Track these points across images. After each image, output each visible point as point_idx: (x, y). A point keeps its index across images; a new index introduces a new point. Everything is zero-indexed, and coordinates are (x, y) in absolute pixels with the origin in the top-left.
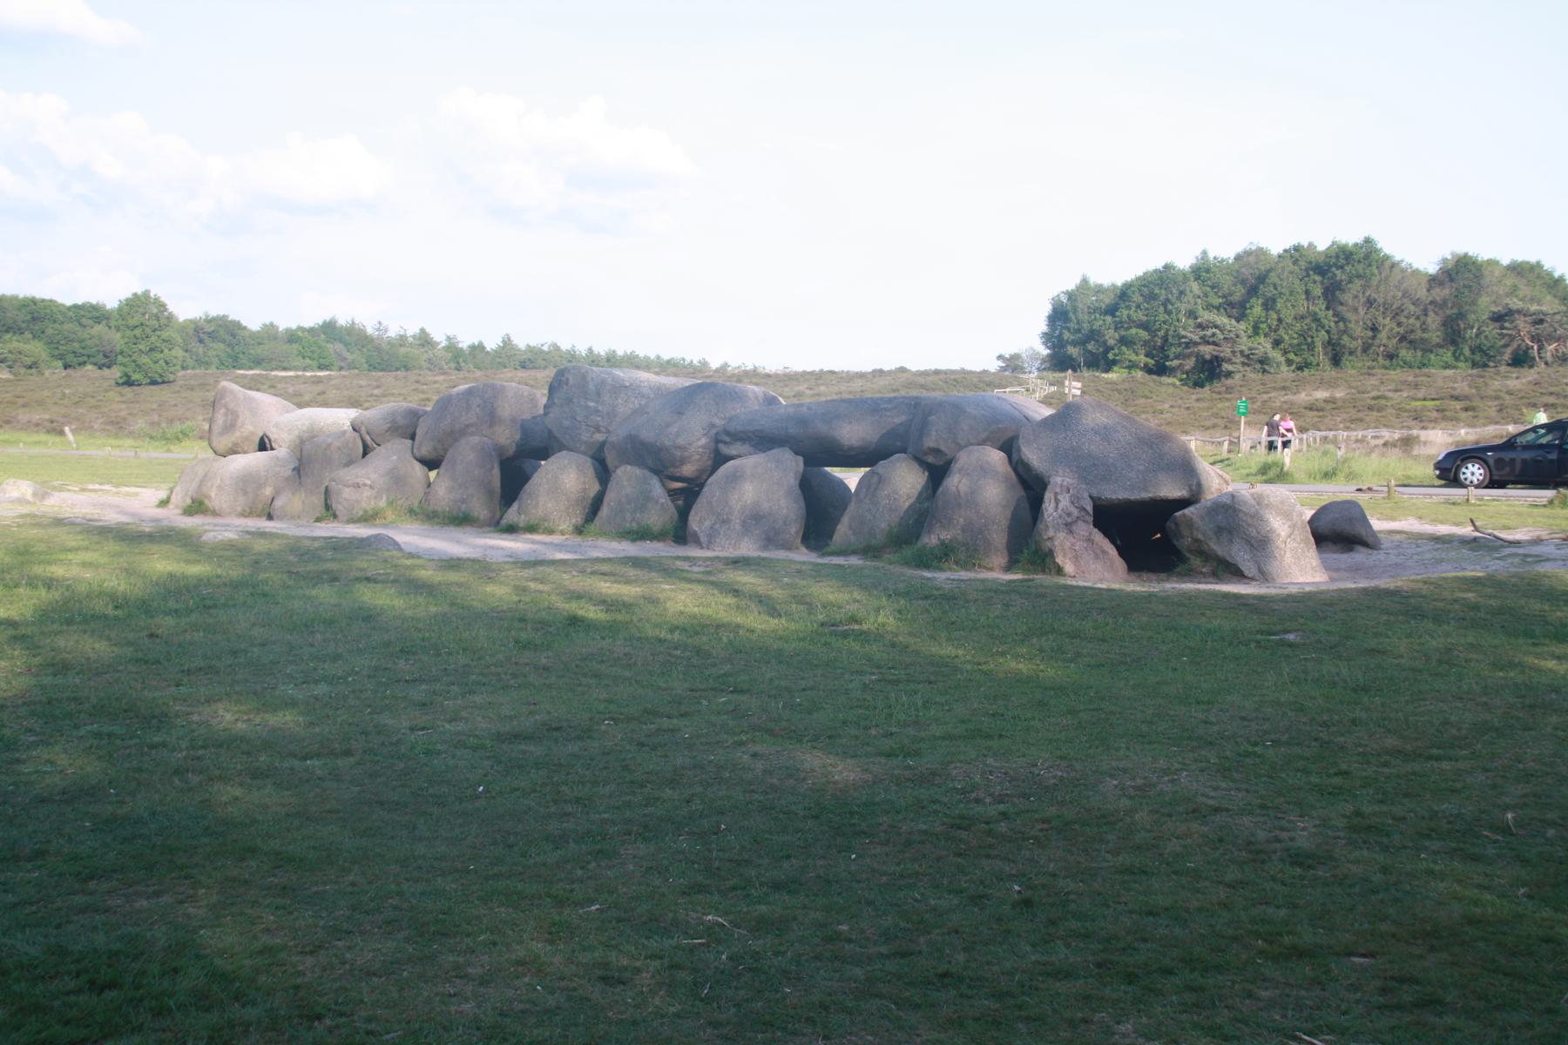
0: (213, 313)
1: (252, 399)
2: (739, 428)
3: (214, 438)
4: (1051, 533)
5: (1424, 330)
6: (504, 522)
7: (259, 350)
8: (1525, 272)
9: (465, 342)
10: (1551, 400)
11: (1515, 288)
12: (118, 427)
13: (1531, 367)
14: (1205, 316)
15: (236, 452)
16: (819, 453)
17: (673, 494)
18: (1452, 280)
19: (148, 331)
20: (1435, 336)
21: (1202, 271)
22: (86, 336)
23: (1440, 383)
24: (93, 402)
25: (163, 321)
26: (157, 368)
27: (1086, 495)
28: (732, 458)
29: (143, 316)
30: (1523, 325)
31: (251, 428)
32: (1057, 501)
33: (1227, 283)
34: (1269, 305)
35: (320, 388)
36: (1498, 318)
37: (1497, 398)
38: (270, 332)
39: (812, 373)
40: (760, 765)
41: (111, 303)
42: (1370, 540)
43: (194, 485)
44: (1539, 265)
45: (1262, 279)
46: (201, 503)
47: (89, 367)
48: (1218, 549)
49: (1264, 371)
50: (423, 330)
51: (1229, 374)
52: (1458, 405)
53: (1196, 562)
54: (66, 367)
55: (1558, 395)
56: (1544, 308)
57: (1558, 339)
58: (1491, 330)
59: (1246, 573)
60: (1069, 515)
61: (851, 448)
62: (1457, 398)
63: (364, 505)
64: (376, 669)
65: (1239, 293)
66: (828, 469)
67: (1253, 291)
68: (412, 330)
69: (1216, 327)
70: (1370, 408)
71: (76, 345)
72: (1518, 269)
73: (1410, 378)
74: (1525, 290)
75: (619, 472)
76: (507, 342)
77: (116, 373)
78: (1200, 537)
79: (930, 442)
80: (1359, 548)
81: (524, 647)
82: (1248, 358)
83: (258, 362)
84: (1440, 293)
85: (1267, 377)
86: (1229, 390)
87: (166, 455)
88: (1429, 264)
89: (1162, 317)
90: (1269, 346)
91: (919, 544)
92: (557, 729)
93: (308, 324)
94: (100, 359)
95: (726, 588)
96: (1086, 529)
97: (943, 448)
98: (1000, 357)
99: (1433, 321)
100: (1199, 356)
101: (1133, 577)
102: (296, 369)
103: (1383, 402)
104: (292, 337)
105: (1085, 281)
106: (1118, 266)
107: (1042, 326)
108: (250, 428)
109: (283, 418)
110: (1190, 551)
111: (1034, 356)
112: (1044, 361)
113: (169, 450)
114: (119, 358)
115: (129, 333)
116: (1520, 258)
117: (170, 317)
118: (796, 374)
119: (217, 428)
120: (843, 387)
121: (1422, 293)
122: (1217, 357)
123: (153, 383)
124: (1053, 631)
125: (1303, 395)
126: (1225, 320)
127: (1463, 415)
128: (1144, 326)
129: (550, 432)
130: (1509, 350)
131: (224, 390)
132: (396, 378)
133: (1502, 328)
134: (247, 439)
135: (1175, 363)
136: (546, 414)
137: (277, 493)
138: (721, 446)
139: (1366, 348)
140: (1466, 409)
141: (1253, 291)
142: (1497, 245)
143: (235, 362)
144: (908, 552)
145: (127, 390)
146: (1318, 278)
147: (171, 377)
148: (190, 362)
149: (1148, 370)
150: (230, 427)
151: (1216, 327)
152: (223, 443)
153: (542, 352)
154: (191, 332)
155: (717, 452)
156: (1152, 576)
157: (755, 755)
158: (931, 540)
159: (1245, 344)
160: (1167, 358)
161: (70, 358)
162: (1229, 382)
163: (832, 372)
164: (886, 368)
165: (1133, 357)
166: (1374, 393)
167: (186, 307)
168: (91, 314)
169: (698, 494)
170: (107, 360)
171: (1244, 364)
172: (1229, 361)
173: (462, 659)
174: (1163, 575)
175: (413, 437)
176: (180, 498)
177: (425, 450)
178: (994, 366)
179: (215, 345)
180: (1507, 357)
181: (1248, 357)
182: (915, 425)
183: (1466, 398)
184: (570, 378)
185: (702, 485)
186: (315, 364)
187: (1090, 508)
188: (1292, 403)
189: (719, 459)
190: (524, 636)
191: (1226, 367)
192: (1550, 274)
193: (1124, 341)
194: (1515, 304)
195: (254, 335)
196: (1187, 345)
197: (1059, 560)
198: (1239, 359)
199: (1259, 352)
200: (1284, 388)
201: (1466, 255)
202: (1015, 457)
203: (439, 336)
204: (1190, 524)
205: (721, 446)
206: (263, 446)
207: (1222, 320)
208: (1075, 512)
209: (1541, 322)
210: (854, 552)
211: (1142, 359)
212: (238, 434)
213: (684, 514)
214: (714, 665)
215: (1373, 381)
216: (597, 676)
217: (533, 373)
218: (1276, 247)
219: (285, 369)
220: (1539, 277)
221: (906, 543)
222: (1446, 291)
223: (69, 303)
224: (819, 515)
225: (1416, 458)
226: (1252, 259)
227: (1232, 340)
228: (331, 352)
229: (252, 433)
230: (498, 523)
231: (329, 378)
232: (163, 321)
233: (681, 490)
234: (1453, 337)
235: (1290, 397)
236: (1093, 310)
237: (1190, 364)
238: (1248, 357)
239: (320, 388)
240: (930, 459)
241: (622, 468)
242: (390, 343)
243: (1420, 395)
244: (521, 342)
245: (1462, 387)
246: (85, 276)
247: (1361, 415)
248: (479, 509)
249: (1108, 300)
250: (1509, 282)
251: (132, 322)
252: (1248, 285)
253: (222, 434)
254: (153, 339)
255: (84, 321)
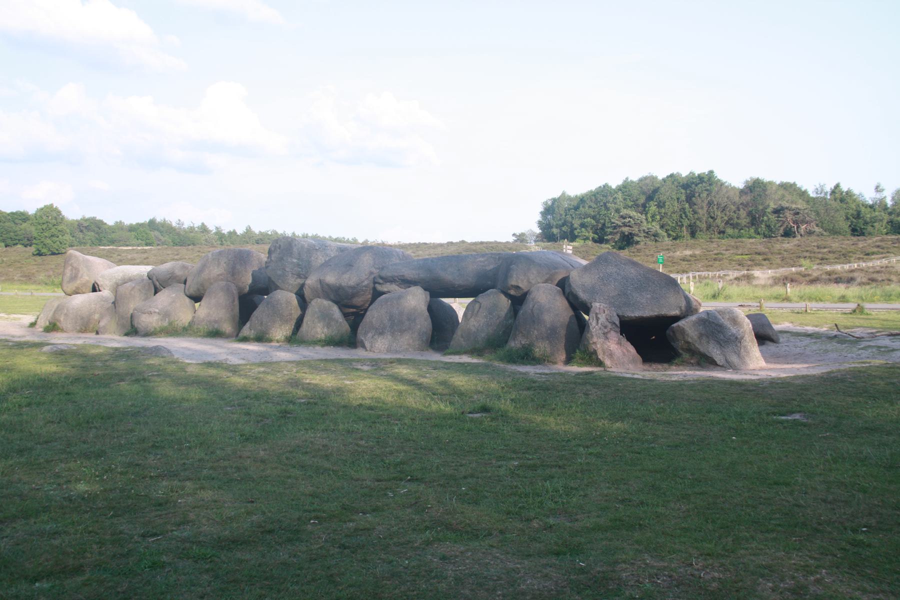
0: (87, 216)
1: (88, 261)
2: (389, 274)
3: (64, 284)
4: (595, 340)
5: (738, 218)
6: (241, 335)
7: (113, 236)
8: (788, 188)
9: (225, 231)
10: (807, 254)
11: (783, 196)
12: (28, 278)
13: (794, 237)
14: (624, 212)
15: (77, 293)
16: (438, 290)
17: (346, 315)
18: (751, 192)
19: (50, 226)
20: (744, 220)
21: (626, 187)
22: (18, 229)
23: (749, 246)
24: (19, 265)
25: (59, 220)
26: (55, 246)
27: (615, 314)
28: (384, 293)
29: (49, 217)
30: (789, 216)
31: (87, 278)
32: (598, 319)
33: (635, 193)
34: (661, 205)
35: (145, 255)
36: (777, 212)
37: (780, 254)
38: (119, 226)
39: (414, 244)
40: (450, 571)
41: (31, 210)
42: (774, 338)
43: (52, 313)
44: (794, 184)
45: (656, 191)
46: (55, 325)
47: (19, 246)
48: (702, 349)
49: (656, 241)
50: (203, 224)
51: (637, 243)
52: (760, 258)
53: (686, 356)
54: (6, 246)
55: (811, 252)
56: (799, 206)
57: (807, 223)
58: (773, 217)
59: (718, 363)
60: (606, 327)
61: (460, 286)
62: (759, 254)
63: (154, 325)
64: (130, 465)
65: (642, 200)
66: (446, 300)
67: (650, 198)
68: (197, 224)
69: (630, 217)
70: (715, 260)
71: (12, 234)
72: (785, 187)
73: (733, 244)
74: (788, 197)
75: (313, 303)
76: (249, 230)
77: (33, 249)
78: (689, 340)
79: (513, 282)
80: (768, 342)
81: (247, 439)
82: (647, 233)
83: (112, 242)
84: (747, 198)
85: (658, 244)
86: (639, 251)
87: (52, 294)
88: (740, 185)
89: (603, 212)
90: (658, 227)
91: (507, 347)
92: (270, 532)
93: (141, 221)
94: (25, 241)
95: (383, 377)
96: (614, 336)
97: (520, 285)
98: (514, 235)
99: (743, 213)
100: (623, 233)
101: (646, 367)
102: (133, 245)
103: (721, 256)
104: (132, 229)
105: (563, 194)
106: (579, 184)
107: (538, 217)
108: (86, 278)
109: (106, 271)
110: (683, 349)
111: (533, 234)
112: (537, 237)
113: (54, 291)
114: (28, 241)
115: (40, 227)
116: (785, 181)
117: (63, 218)
118: (406, 245)
119: (67, 278)
120: (432, 251)
121: (737, 199)
122: (631, 234)
123: (53, 254)
124: (628, 415)
125: (678, 253)
126: (635, 214)
127: (764, 263)
128: (594, 217)
129: (269, 278)
130: (782, 228)
131: (71, 255)
132: (188, 250)
133: (779, 217)
134: (84, 285)
135: (610, 237)
136: (267, 267)
137: (102, 317)
138: (377, 285)
139: (709, 227)
140: (765, 260)
141: (650, 198)
142: (774, 173)
143: (100, 242)
144: (501, 352)
145: (38, 258)
146: (683, 191)
147: (63, 251)
148: (76, 243)
149: (595, 241)
150: (74, 278)
151: (630, 217)
152: (70, 287)
153: (267, 235)
154: (76, 226)
155: (374, 289)
156: (659, 366)
157: (444, 558)
158: (515, 344)
159: (645, 226)
160: (605, 234)
161: (9, 242)
162: (638, 246)
163: (425, 244)
164: (454, 241)
165: (587, 234)
166: (715, 252)
167: (73, 213)
168: (22, 217)
169: (363, 316)
170: (28, 242)
171: (645, 237)
172: (637, 235)
173: (199, 453)
174: (666, 365)
175: (185, 283)
176: (43, 323)
177: (192, 291)
178: (511, 239)
179: (89, 233)
180: (781, 231)
181: (647, 233)
182: (491, 274)
183: (764, 254)
184: (283, 247)
185: (366, 310)
186: (144, 242)
187: (618, 323)
188: (673, 257)
189: (377, 294)
190: (247, 429)
191: (636, 238)
192: (799, 189)
193: (583, 225)
194: (785, 204)
195: (110, 227)
196: (615, 228)
197: (600, 357)
198: (642, 234)
199: (653, 230)
200: (668, 249)
201: (758, 179)
202: (567, 290)
203: (212, 227)
204: (682, 331)
205: (377, 285)
206: (94, 289)
207: (633, 213)
208: (610, 326)
209: (798, 213)
210: (465, 353)
211: (591, 235)
212: (78, 282)
213: (354, 327)
214: (392, 453)
215: (714, 245)
216: (303, 467)
217: (263, 246)
218: (661, 175)
219: (127, 246)
220: (795, 190)
221: (499, 346)
222: (749, 198)
223: (8, 212)
224: (441, 332)
225: (756, 286)
226: (648, 181)
227: (639, 225)
228: (153, 235)
229: (88, 281)
230: (237, 335)
231: (151, 250)
232: (59, 220)
233: (353, 314)
234: (754, 220)
235: (671, 254)
236: (567, 210)
237: (617, 237)
238: (647, 233)
239: (145, 255)
240: (512, 292)
241: (315, 300)
242: (185, 230)
243: (739, 252)
244: (256, 229)
245: (761, 248)
246: (27, 199)
247: (711, 263)
248: (227, 328)
249: (575, 203)
250: (781, 192)
251: (41, 221)
252: (646, 195)
253: (69, 282)
254: (53, 230)
255: (17, 221)
